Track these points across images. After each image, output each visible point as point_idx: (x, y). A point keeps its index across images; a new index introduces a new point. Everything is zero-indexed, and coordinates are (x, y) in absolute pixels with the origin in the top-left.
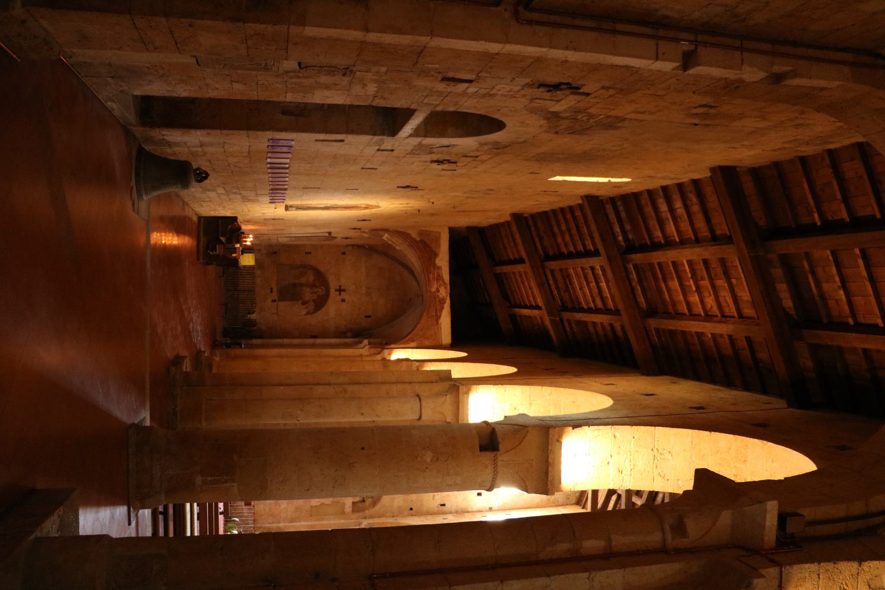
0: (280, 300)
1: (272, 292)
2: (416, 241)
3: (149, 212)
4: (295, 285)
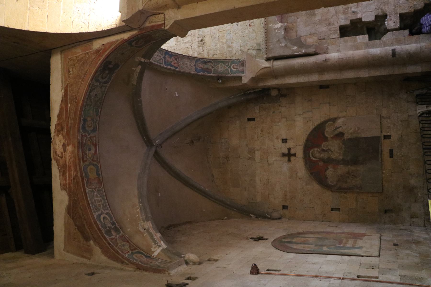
0: (377, 139)
1: (391, 151)
2: (97, 242)
4: (355, 162)
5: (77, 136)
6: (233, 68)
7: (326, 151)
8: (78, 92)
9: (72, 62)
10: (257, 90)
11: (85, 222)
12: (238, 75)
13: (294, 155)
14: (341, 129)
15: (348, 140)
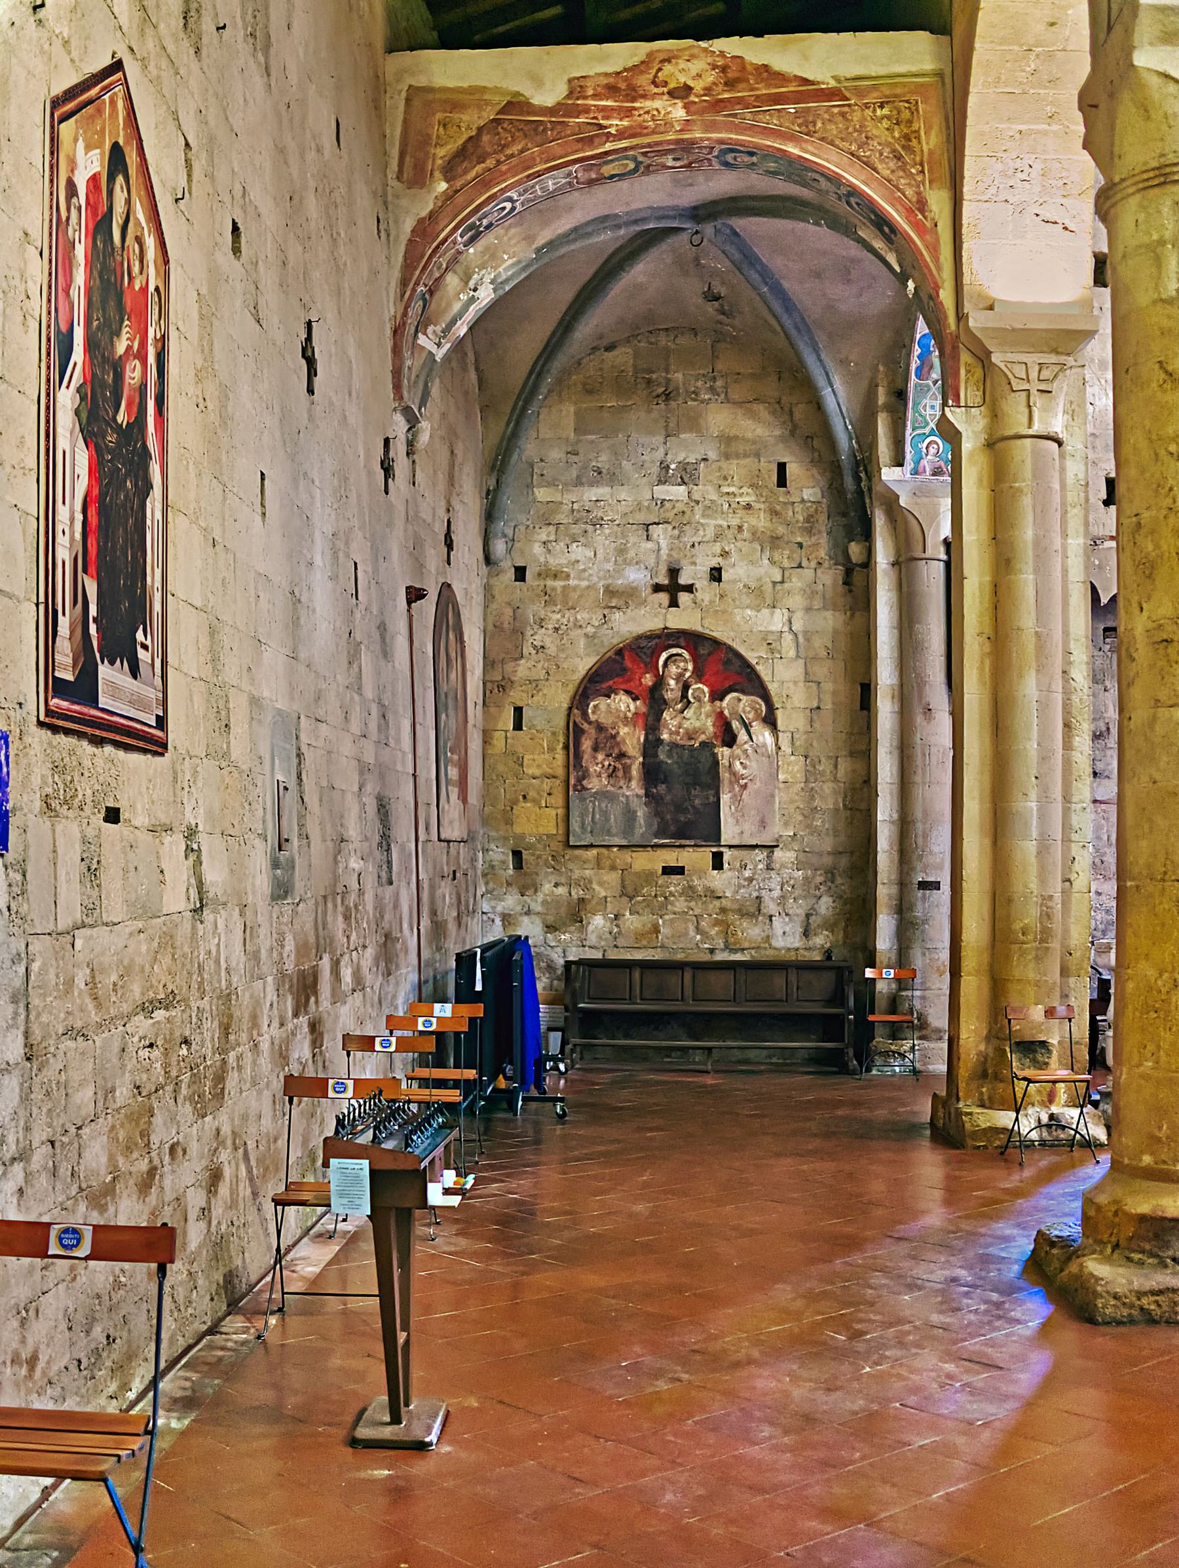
0: (713, 834)
3: (200, 884)
4: (652, 774)
5: (708, 139)
6: (930, 443)
7: (684, 696)
8: (822, 139)
9: (906, 115)
10: (867, 501)
11: (490, 163)
12: (908, 456)
13: (674, 603)
14: (746, 738)
15: (715, 756)
